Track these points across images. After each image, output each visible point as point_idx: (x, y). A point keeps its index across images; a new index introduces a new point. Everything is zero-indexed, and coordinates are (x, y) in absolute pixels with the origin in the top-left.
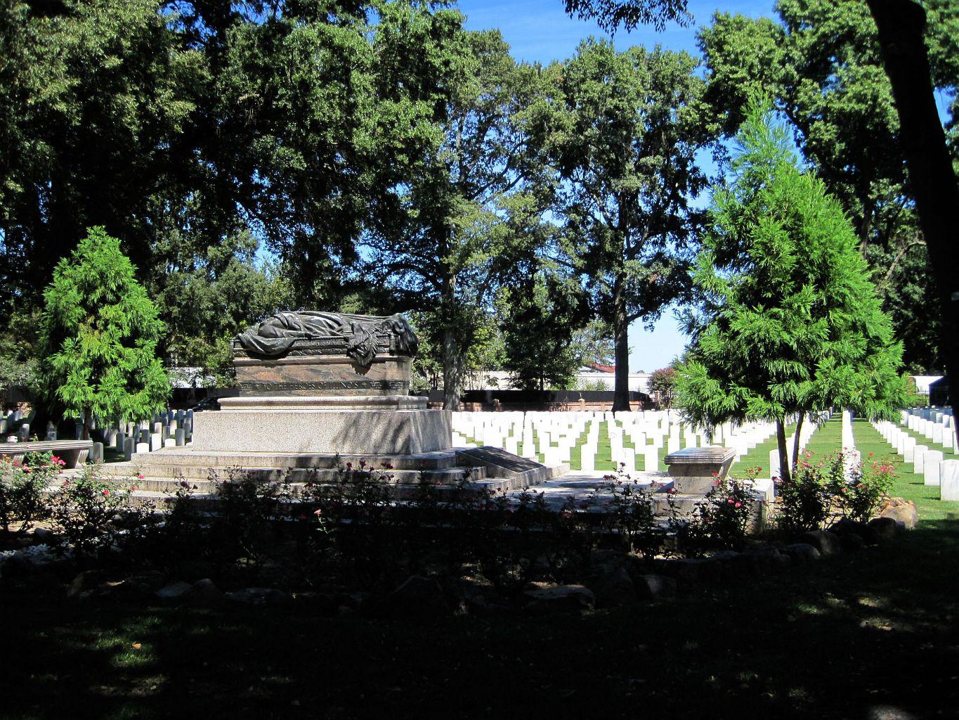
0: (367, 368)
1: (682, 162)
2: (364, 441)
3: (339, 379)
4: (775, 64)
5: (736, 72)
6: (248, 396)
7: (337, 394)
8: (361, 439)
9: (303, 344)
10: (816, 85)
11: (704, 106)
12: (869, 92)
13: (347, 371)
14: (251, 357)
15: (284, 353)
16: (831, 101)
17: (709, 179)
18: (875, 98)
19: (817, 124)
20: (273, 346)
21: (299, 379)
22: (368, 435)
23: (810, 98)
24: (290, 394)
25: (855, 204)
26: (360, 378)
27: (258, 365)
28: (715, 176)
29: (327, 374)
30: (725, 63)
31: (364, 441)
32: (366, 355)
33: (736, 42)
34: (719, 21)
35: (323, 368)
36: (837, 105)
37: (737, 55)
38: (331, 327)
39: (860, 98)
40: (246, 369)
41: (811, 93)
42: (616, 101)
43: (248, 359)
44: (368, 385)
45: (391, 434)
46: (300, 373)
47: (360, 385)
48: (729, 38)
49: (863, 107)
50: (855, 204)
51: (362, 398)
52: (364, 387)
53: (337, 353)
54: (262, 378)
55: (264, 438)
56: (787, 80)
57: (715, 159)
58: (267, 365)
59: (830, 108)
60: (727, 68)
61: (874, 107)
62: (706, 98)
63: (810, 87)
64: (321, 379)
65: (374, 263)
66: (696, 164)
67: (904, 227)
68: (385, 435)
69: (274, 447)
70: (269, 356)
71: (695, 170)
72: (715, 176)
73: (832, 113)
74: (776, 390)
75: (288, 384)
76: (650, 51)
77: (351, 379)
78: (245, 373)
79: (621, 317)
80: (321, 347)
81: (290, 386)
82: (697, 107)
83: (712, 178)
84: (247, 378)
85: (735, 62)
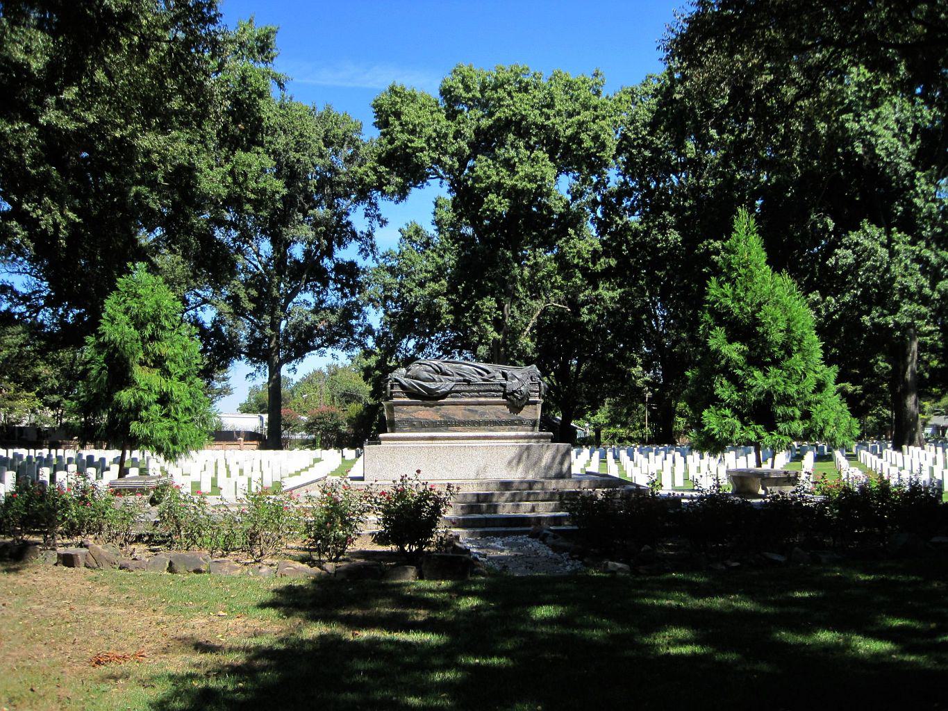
0: (520, 409)
1: (341, 215)
2: (536, 463)
3: (495, 418)
4: (450, 138)
5: (413, 141)
6: (406, 431)
7: (491, 431)
8: (533, 462)
9: (463, 388)
10: (490, 162)
11: (382, 169)
12: (539, 174)
13: (503, 412)
14: (410, 398)
15: (444, 395)
16: (503, 177)
17: (359, 234)
18: (543, 179)
19: (491, 196)
20: (437, 389)
21: (456, 417)
22: (540, 459)
23: (485, 172)
24: (447, 430)
25: (514, 268)
26: (514, 417)
27: (417, 404)
28: (365, 231)
29: (483, 414)
30: (402, 132)
31: (536, 463)
32: (522, 399)
33: (410, 113)
34: (396, 93)
35: (476, 408)
36: (509, 182)
37: (414, 126)
38: (480, 374)
39: (531, 178)
40: (405, 408)
41: (486, 168)
42: (298, 155)
43: (407, 400)
44: (521, 422)
45: (558, 460)
46: (458, 413)
47: (510, 423)
48: (405, 109)
49: (535, 186)
50: (514, 268)
51: (513, 434)
52: (516, 424)
53: (493, 396)
54: (420, 417)
55: (438, 468)
56: (458, 154)
57: (367, 215)
58: (426, 406)
59: (503, 184)
60: (405, 136)
61: (540, 187)
62: (381, 161)
63: (484, 163)
64: (477, 418)
65: (30, 294)
66: (350, 219)
67: (556, 291)
68: (554, 458)
69: (448, 475)
70: (430, 398)
71: (349, 223)
72: (365, 231)
73: (505, 188)
74: (781, 426)
75: (446, 422)
76: (321, 110)
77: (504, 418)
78: (403, 412)
79: (276, 358)
80: (478, 391)
81: (448, 424)
82: (374, 169)
83: (362, 233)
84: (404, 416)
85: (413, 132)
